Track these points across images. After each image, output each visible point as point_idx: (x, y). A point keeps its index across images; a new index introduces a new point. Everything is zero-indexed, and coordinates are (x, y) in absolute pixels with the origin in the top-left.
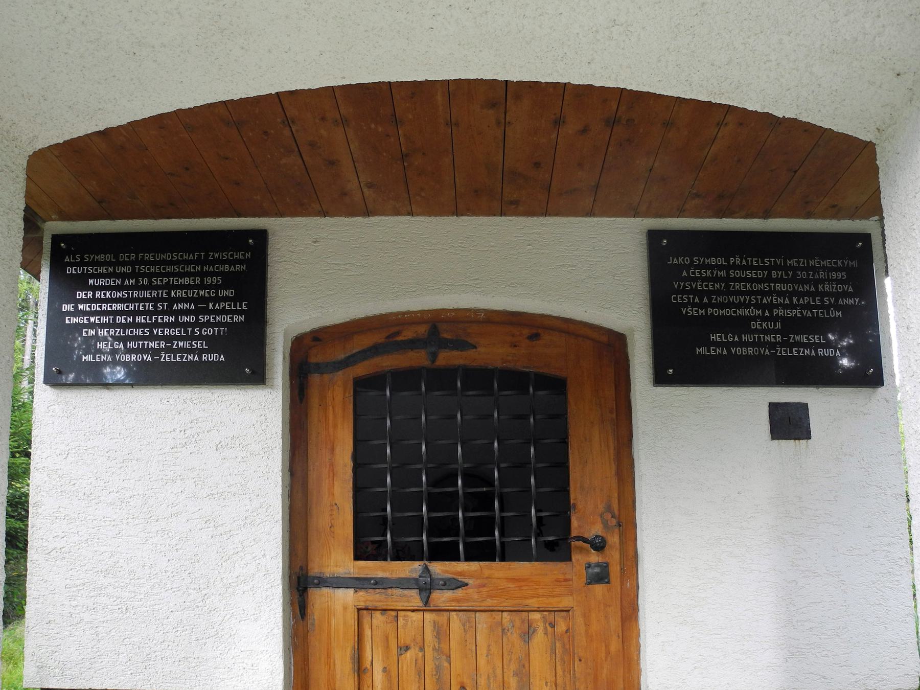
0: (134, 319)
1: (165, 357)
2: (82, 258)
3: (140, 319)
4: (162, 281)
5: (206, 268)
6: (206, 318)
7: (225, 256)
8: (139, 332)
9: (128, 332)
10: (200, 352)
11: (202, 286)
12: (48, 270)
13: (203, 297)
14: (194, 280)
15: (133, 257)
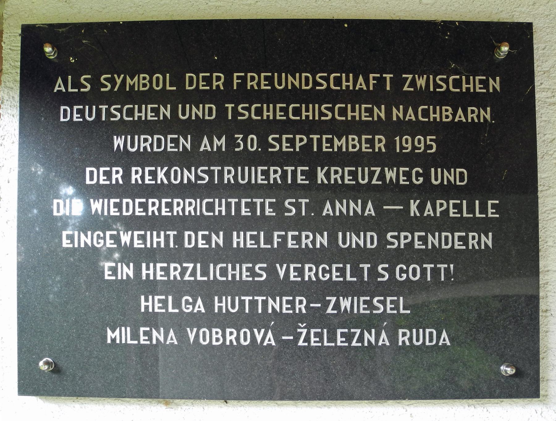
0: (228, 239)
1: (309, 337)
2: (95, 83)
3: (242, 240)
4: (291, 142)
5: (397, 113)
6: (405, 238)
7: (444, 83)
8: (242, 272)
9: (215, 271)
10: (394, 323)
11: (391, 158)
12: (16, 112)
13: (395, 186)
14: (371, 142)
15: (219, 82)
